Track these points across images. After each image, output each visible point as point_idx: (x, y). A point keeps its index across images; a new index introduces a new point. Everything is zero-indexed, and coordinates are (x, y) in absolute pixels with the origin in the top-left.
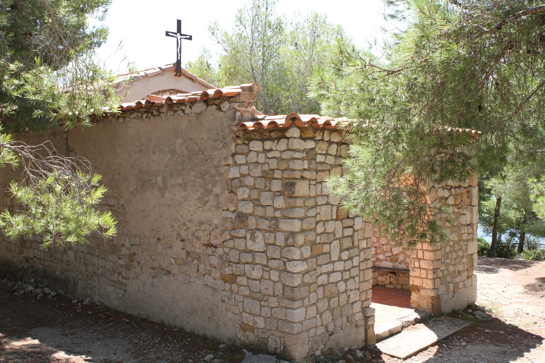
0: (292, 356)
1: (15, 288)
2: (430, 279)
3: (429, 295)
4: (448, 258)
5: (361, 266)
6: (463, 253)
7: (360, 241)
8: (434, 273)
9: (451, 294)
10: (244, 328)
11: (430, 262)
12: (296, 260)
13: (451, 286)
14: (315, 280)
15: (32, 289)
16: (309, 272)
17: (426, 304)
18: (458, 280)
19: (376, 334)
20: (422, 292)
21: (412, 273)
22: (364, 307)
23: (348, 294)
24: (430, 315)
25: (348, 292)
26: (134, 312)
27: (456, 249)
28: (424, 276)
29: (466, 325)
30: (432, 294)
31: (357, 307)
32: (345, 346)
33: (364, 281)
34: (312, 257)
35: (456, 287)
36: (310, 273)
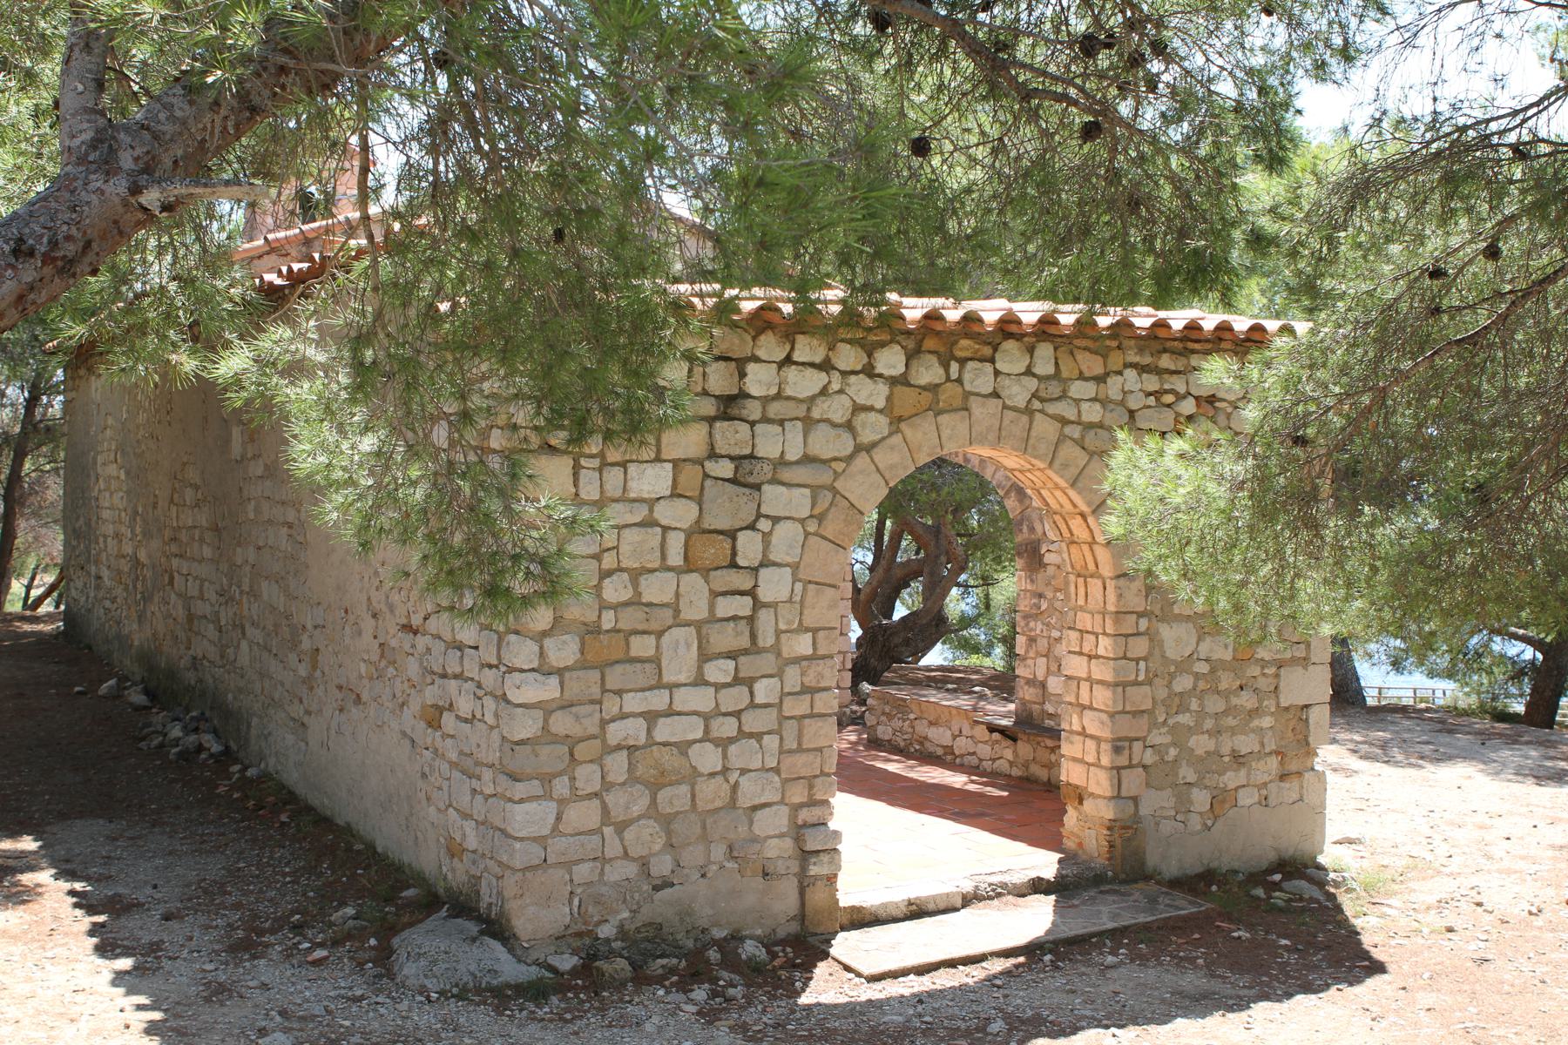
0: (512, 927)
1: (146, 731)
3: (1102, 814)
4: (1183, 708)
6: (1260, 701)
7: (784, 637)
8: (1117, 750)
9: (1195, 823)
10: (455, 850)
11: (1104, 717)
12: (522, 671)
13: (1201, 799)
14: (595, 730)
15: (181, 734)
16: (572, 705)
17: (1094, 842)
18: (1231, 779)
19: (841, 904)
20: (1088, 805)
21: (1066, 749)
22: (800, 822)
23: (732, 781)
24: (1096, 875)
25: (734, 776)
26: (314, 800)
27: (1223, 686)
28: (1090, 759)
29: (1182, 912)
30: (1107, 812)
31: (773, 822)
32: (717, 924)
33: (800, 750)
34: (582, 665)
35: (1223, 801)
36: (574, 709)
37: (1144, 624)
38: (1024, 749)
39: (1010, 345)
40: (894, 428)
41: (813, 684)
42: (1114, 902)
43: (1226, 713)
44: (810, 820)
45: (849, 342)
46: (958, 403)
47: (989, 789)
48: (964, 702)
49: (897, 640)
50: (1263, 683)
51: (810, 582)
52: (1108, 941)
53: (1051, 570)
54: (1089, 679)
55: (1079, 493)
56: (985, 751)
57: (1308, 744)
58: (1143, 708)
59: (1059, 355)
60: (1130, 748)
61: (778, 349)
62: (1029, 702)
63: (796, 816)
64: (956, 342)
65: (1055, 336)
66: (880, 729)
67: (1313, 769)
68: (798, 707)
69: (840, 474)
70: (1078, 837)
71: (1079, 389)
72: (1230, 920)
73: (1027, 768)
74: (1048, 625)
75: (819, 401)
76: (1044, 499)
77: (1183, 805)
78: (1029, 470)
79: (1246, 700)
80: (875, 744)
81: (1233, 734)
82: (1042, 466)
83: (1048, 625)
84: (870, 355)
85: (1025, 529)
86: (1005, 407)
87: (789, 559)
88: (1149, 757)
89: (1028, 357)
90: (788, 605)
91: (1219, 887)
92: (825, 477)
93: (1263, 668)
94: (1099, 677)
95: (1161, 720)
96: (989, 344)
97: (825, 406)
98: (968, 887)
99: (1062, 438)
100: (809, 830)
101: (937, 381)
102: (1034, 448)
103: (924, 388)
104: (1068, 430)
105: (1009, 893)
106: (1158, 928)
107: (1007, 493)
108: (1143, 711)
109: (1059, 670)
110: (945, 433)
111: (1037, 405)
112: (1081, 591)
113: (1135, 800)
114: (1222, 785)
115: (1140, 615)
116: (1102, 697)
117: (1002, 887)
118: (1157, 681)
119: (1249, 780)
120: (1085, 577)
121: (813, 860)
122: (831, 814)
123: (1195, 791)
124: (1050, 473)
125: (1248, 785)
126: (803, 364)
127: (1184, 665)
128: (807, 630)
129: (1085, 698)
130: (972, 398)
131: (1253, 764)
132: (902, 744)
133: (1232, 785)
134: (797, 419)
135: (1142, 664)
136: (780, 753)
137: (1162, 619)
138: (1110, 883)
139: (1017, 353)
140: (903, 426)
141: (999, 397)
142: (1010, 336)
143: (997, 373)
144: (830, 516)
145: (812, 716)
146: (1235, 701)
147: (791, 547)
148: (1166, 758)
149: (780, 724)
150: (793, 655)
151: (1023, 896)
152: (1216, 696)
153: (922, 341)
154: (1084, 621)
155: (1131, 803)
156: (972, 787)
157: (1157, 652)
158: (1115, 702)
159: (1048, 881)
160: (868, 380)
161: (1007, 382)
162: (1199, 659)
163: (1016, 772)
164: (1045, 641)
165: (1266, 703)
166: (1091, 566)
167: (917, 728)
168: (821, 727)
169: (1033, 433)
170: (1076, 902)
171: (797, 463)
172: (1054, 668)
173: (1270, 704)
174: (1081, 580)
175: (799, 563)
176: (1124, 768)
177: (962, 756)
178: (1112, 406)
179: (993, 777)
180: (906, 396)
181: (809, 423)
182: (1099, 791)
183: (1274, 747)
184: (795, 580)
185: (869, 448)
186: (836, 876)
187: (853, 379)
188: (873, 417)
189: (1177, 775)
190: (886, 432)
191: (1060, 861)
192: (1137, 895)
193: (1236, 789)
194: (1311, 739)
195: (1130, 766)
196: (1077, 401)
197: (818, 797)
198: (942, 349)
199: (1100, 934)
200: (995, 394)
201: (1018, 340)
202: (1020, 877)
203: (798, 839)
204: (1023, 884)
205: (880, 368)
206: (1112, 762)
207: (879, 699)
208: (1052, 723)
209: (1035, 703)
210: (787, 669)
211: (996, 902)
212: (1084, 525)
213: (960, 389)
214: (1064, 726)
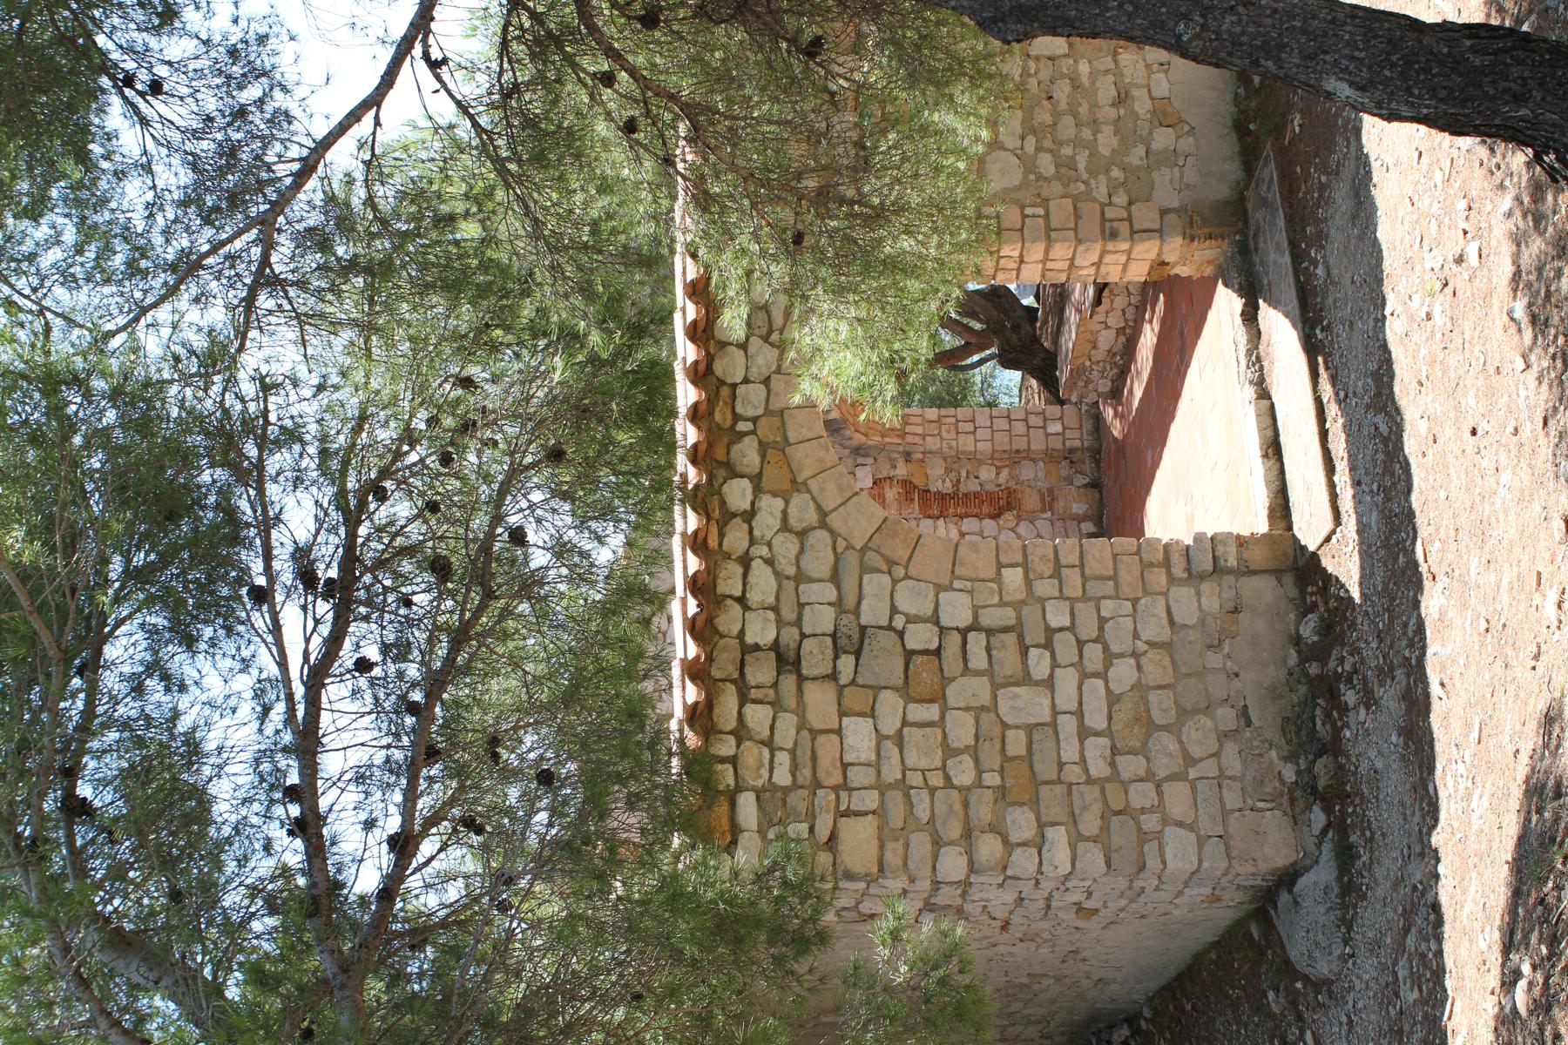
4: (1071, 164)
6: (1063, 76)
8: (1114, 235)
9: (1186, 144)
11: (1081, 249)
13: (1163, 139)
18: (1142, 106)
20: (1168, 258)
22: (1185, 575)
27: (1048, 119)
28: (1123, 258)
33: (1115, 578)
35: (1165, 114)
39: (718, 367)
41: (1051, 566)
43: (1075, 115)
44: (1183, 564)
45: (722, 535)
46: (776, 420)
48: (1072, 316)
54: (1044, 262)
58: (1071, 208)
64: (718, 425)
68: (1073, 578)
75: (779, 568)
77: (1171, 157)
79: (1062, 91)
80: (1116, 394)
84: (734, 515)
86: (778, 371)
88: (1121, 199)
92: (851, 561)
93: (1030, 75)
97: (784, 561)
98: (1250, 392)
101: (756, 444)
103: (763, 457)
105: (1257, 348)
111: (775, 337)
113: (1164, 212)
118: (1044, 195)
119: (1143, 86)
126: (744, 585)
128: (999, 573)
133: (1148, 104)
135: (1028, 211)
139: (726, 360)
140: (800, 480)
143: (746, 381)
144: (888, 553)
145: (1082, 566)
146: (1063, 105)
147: (919, 594)
149: (1090, 599)
151: (1259, 332)
157: (1015, 195)
158: (1065, 240)
159: (1245, 305)
160: (757, 517)
161: (754, 370)
165: (1065, 70)
170: (1265, 282)
171: (839, 588)
177: (1126, 321)
181: (800, 578)
182: (1156, 250)
184: (950, 588)
185: (823, 514)
186: (1238, 537)
187: (757, 533)
189: (1138, 168)
190: (807, 496)
193: (1152, 99)
195: (1130, 220)
197: (1160, 556)
198: (726, 441)
199: (1296, 272)
200: (766, 381)
203: (1202, 577)
204: (1248, 333)
206: (1125, 240)
211: (1265, 364)
213: (763, 421)
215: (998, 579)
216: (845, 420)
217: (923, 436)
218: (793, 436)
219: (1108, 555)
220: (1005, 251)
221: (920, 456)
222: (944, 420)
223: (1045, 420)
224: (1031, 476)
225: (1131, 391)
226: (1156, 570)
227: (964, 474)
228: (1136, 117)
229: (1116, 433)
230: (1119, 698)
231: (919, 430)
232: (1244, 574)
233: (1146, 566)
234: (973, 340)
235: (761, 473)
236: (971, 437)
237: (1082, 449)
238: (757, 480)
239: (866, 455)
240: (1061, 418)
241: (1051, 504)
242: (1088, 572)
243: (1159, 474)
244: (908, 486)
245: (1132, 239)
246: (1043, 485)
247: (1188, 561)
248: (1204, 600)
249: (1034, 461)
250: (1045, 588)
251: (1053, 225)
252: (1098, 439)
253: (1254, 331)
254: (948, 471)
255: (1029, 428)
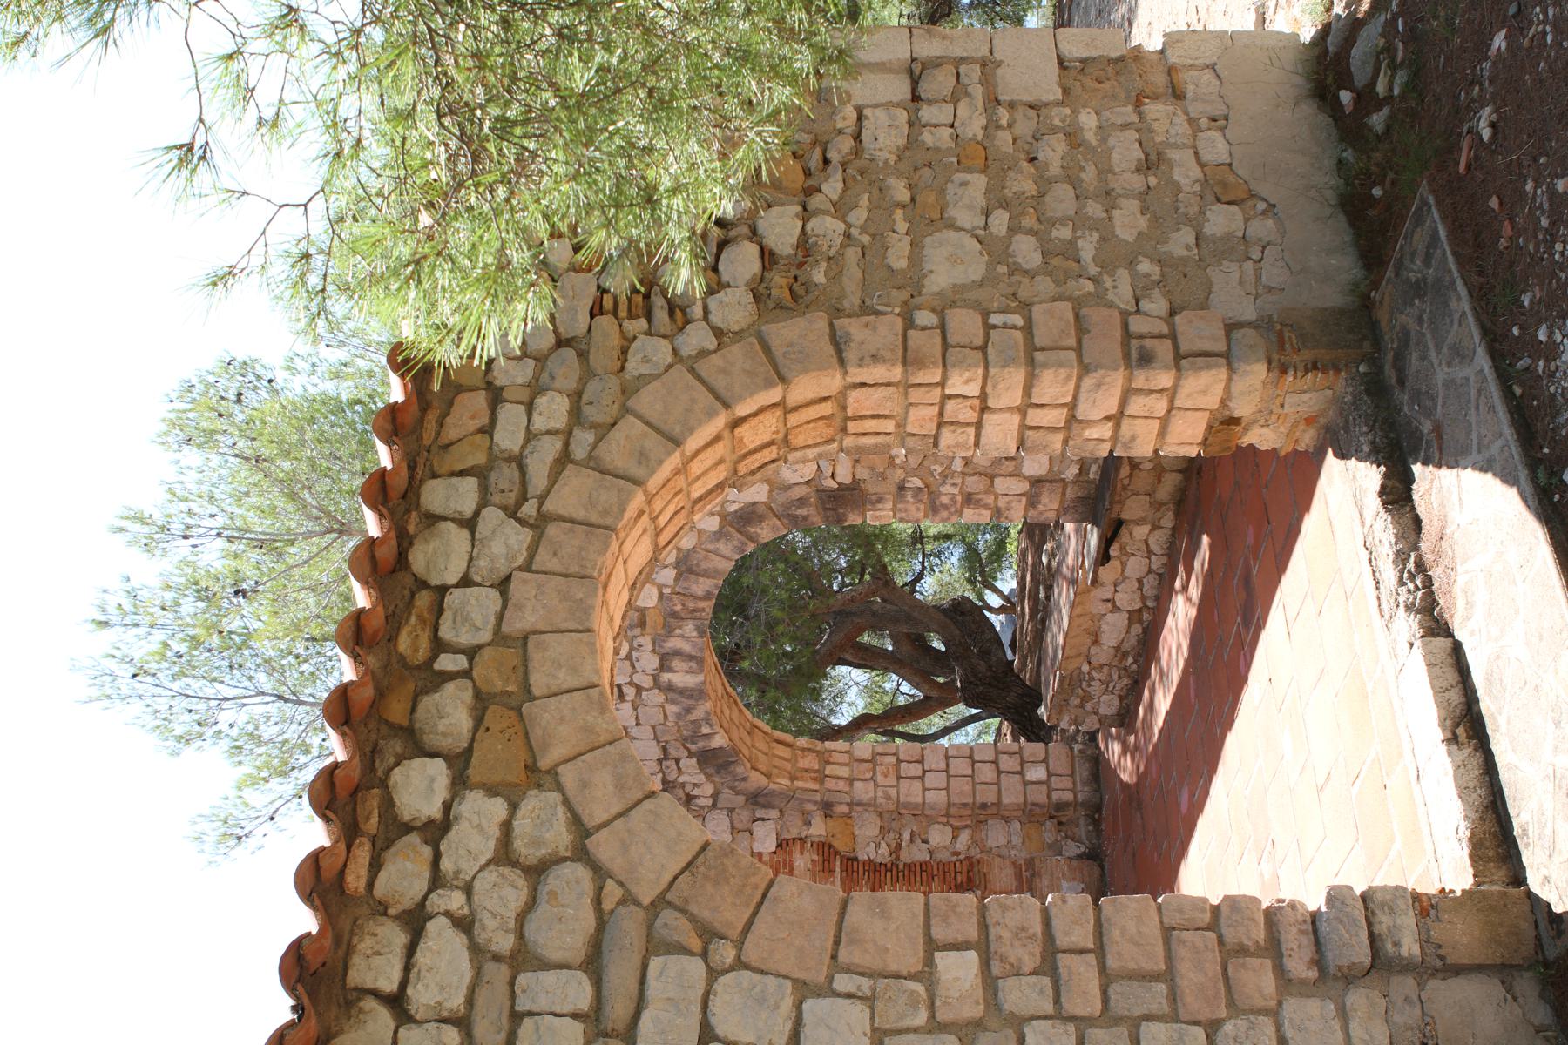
2: (1178, 379)
3: (1259, 385)
4: (1070, 251)
5: (1080, 1011)
6: (1054, 130)
8: (1146, 359)
9: (1263, 228)
11: (1088, 382)
13: (1221, 220)
17: (1306, 397)
18: (1186, 173)
20: (1242, 408)
21: (1143, 449)
22: (1313, 974)
24: (1368, 392)
27: (1029, 187)
28: (1161, 406)
29: (1442, 233)
30: (1255, 374)
33: (1168, 976)
35: (1224, 185)
37: (925, 318)
38: (1133, 508)
39: (419, 558)
40: (549, 779)
41: (1037, 949)
42: (1424, 357)
43: (1074, 183)
44: (1308, 952)
45: (376, 866)
46: (511, 655)
47: (1197, 564)
48: (1063, 595)
49: (982, 667)
50: (1026, 125)
51: (834, 957)
52: (1521, 364)
53: (862, 473)
54: (1022, 411)
55: (691, 431)
56: (1136, 566)
57: (1122, 59)
58: (1070, 316)
59: (444, 470)
60: (1141, 337)
61: (370, 1026)
62: (1062, 502)
63: (1303, 982)
64: (402, 658)
65: (411, 478)
66: (1103, 710)
67: (1162, 52)
68: (1082, 975)
69: (627, 891)
70: (1295, 425)
71: (508, 436)
72: (1453, 148)
73: (1161, 504)
74: (944, 476)
75: (481, 937)
76: (711, 491)
77: (1236, 248)
78: (654, 519)
79: (1053, 152)
80: (1125, 718)
81: (1111, 171)
82: (638, 500)
83: (944, 476)
84: (407, 828)
85: (802, 512)
86: (527, 567)
87: (787, 1004)
88: (1156, 305)
89: (443, 525)
90: (879, 1005)
91: (1374, 184)
92: (629, 925)
93: (999, 127)
94: (1020, 393)
95: (1090, 287)
96: (413, 595)
97: (491, 923)
98: (1408, 625)
99: (594, 463)
100: (1330, 955)
101: (468, 696)
102: (606, 512)
103: (478, 721)
104: (579, 453)
105: (1416, 548)
106: (1481, 273)
107: (751, 538)
108: (1077, 316)
109: (1012, 459)
110: (565, 679)
111: (529, 509)
112: (870, 425)
113: (1231, 328)
114: (1197, 187)
115: (909, 324)
116: (1054, 386)
117: (1405, 561)
118: (1023, 294)
119: (1184, 146)
120: (847, 419)
121: (1389, 947)
122: (1293, 905)
123: (1208, 230)
124: (653, 483)
125: (1195, 147)
126: (407, 969)
127: (996, 250)
128: (929, 962)
129: (1057, 417)
130: (505, 629)
131: (1159, 139)
132: (1125, 681)
133: (1197, 172)
134: (512, 983)
135: (995, 319)
136: (1176, 1019)
137: (918, 288)
138: (1380, 369)
139: (434, 544)
140: (544, 763)
141: (508, 578)
142: (402, 560)
143: (466, 582)
144: (706, 914)
145: (1100, 950)
146: (1055, 169)
147: (762, 1001)
148: (1156, 277)
149: (1117, 1021)
150: (980, 992)
151: (1417, 522)
152: (1048, 198)
153: (391, 726)
154: (921, 419)
155: (1238, 335)
156: (1195, 591)
157: (972, 295)
158: (1061, 365)
159: (1386, 476)
160: (452, 834)
161: (482, 563)
162: (986, 227)
163: (1168, 521)
164: (969, 480)
165: (1057, 122)
166: (826, 409)
167: (1103, 660)
168: (1123, 931)
169: (580, 514)
170: (1427, 427)
171: (598, 984)
172: (1009, 467)
173: (1058, 116)
174: (852, 427)
175: (795, 981)
176: (1176, 346)
177: (1143, 598)
178: (545, 376)
179: (1177, 556)
180: (494, 757)
181: (523, 958)
182: (1218, 391)
183: (1130, 108)
184: (826, 990)
185: (581, 830)
186: (1417, 897)
187: (446, 865)
188: (523, 825)
189: (1183, 260)
190: (554, 797)
191: (1342, 455)
192: (1407, 319)
193: (1202, 165)
194: (1114, 54)
195: (1173, 336)
196: (530, 436)
197: (1260, 934)
198: (411, 686)
199: (1505, 379)
200: (503, 585)
201: (411, 544)
202: (1383, 530)
203: (1349, 978)
204: (1396, 522)
205: (432, 809)
206: (1166, 368)
207: (1060, 712)
208: (1094, 468)
209: (1064, 494)
210: (1007, 1007)
211: (1436, 574)
212: (754, 422)
213: (487, 653)
214: (1103, 451)
215: (927, 974)
216: (736, 751)
217: (850, 781)
218: (538, 682)
219: (1153, 929)
220: (956, 385)
221: (845, 809)
222: (879, 759)
223: (1022, 763)
224: (1002, 841)
225: (1151, 707)
226: (1254, 962)
227: (906, 836)
228: (1178, 189)
229: (1125, 777)
230: (851, 785)
231: (844, 772)
232: (1435, 973)
233: (1231, 952)
234: (934, 694)
235: (469, 751)
236: (918, 784)
237: (1075, 804)
238: (460, 764)
239: (768, 806)
240: (1045, 761)
241: (1030, 881)
242: (1112, 963)
243: (1203, 823)
244: (826, 851)
245: (1178, 368)
246: (1020, 855)
247: (1318, 943)
248: (1354, 1027)
249: (1007, 820)
250: (1023, 995)
251: (1038, 342)
252: (1098, 790)
253: (1407, 520)
254: (884, 831)
255: (999, 772)
